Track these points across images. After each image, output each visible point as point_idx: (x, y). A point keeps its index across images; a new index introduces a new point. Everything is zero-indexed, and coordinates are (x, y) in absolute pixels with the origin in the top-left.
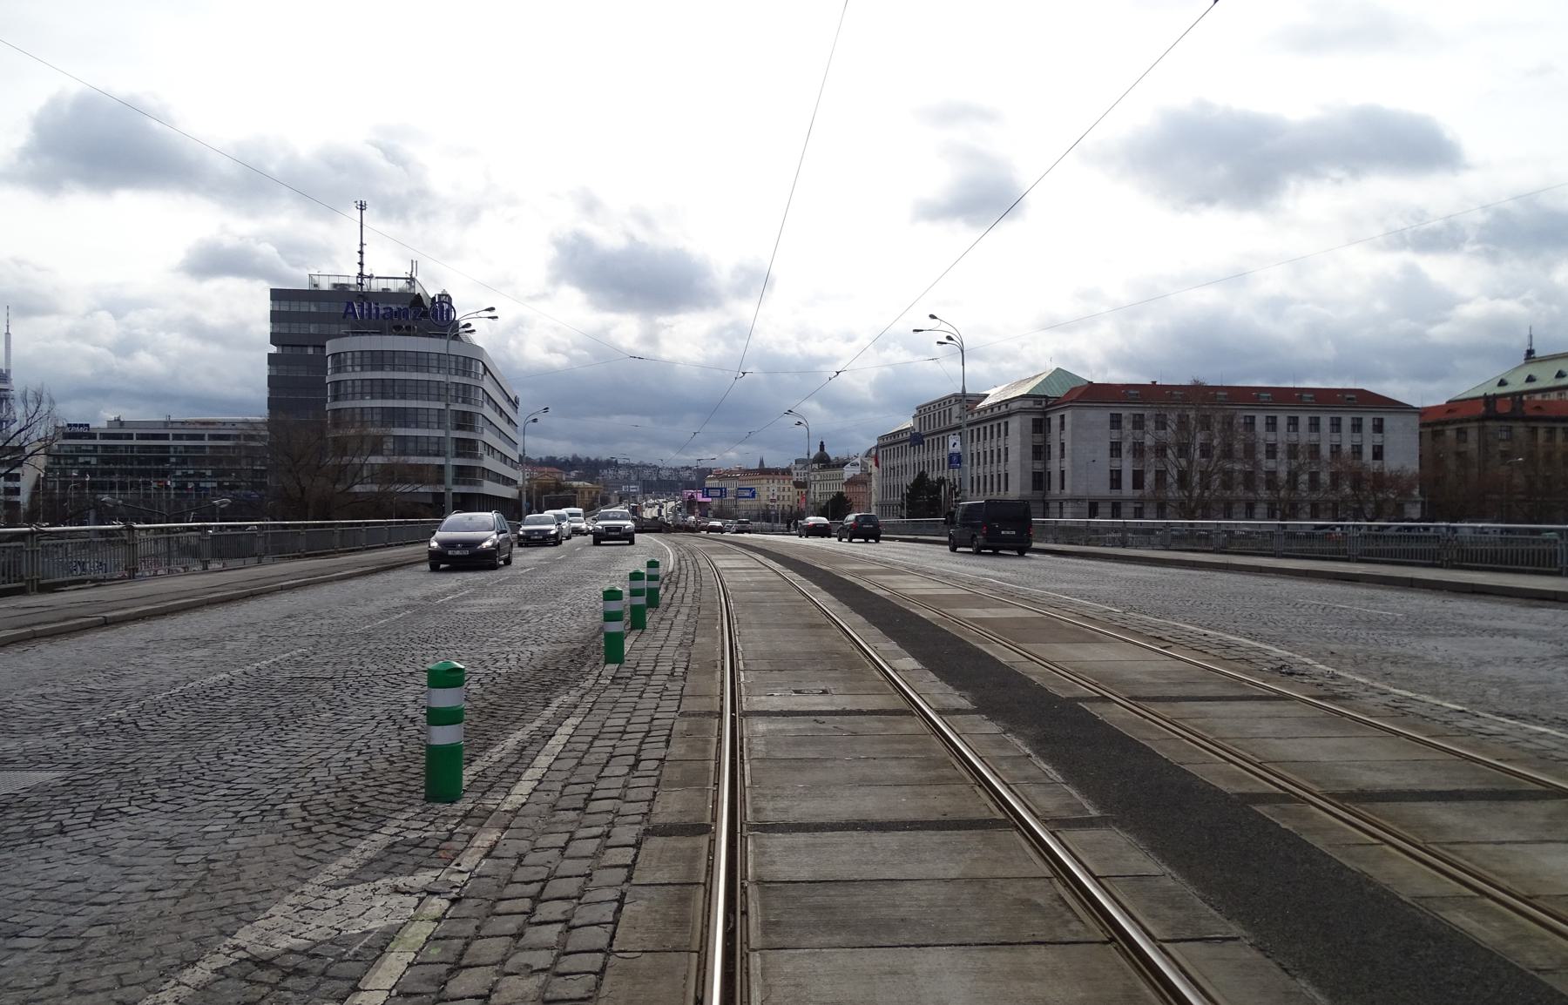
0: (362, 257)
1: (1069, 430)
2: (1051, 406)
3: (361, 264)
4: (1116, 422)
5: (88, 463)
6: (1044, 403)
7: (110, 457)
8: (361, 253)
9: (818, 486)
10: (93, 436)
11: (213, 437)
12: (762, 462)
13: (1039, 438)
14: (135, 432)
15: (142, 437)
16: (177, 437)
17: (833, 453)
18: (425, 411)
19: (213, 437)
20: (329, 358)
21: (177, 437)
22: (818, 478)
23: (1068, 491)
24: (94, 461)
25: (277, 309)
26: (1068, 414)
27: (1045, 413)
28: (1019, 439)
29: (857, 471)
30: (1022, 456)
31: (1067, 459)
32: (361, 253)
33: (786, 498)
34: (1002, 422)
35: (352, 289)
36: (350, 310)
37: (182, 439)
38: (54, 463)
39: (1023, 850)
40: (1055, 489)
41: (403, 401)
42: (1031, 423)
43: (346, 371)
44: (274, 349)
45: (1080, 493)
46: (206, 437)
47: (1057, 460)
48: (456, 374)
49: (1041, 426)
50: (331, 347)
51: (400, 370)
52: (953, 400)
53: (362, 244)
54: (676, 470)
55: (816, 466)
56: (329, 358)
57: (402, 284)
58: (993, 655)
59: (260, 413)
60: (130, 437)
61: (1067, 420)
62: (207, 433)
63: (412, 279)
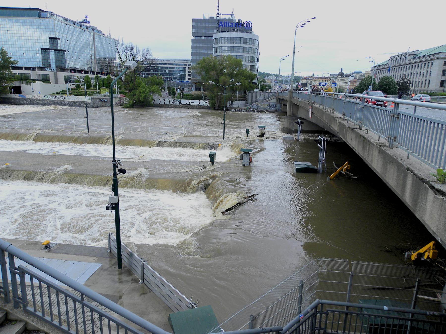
0: (218, 7)
3: (218, 10)
8: (218, 6)
9: (339, 83)
11: (170, 64)
12: (313, 75)
16: (161, 64)
17: (345, 72)
18: (242, 57)
19: (170, 64)
20: (214, 40)
21: (161, 64)
22: (339, 80)
25: (193, 52)
29: (353, 78)
32: (218, 6)
34: (430, 62)
36: (221, 24)
41: (236, 53)
43: (219, 44)
44: (193, 38)
46: (168, 64)
48: (251, 45)
50: (214, 36)
52: (408, 54)
55: (339, 76)
56: (214, 40)
58: (342, 138)
59: (189, 57)
60: (176, 64)
62: (168, 63)
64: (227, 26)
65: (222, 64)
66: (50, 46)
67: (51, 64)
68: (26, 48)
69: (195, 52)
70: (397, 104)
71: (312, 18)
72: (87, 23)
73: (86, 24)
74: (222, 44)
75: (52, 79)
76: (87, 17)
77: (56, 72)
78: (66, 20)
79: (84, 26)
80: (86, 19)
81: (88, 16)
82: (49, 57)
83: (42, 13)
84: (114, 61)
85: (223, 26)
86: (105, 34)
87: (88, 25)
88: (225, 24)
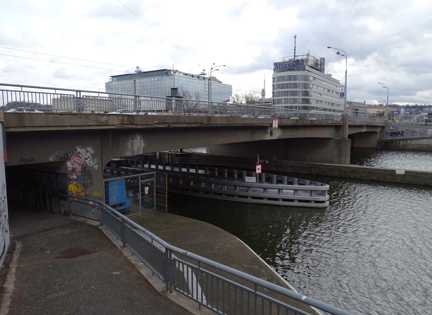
3: (295, 53)
8: (295, 50)
14: (263, 101)
53: (295, 47)
64: (281, 67)
65: (252, 98)
66: (106, 90)
70: (308, 112)
72: (205, 75)
74: (276, 82)
76: (204, 70)
78: (186, 74)
79: (201, 77)
80: (203, 72)
81: (206, 69)
85: (279, 67)
86: (222, 81)
88: (280, 66)
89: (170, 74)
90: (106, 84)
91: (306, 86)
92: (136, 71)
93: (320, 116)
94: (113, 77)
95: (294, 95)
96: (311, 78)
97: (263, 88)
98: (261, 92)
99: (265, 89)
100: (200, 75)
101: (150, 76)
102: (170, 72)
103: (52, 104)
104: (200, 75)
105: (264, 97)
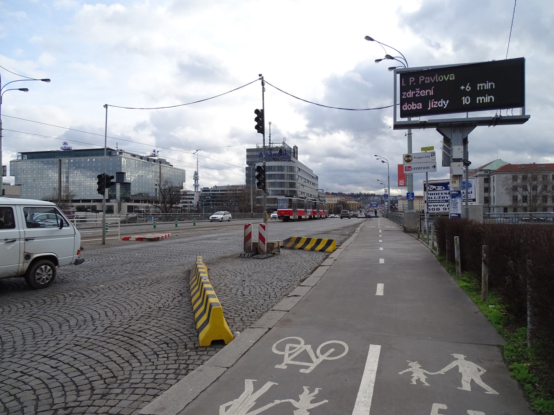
1: (496, 182)
2: (491, 173)
3: (270, 140)
4: (515, 178)
5: (208, 198)
6: (489, 172)
7: (214, 196)
8: (270, 137)
10: (209, 191)
11: (221, 191)
13: (487, 185)
14: (219, 189)
15: (221, 191)
23: (495, 203)
24: (210, 198)
25: (248, 154)
26: (495, 176)
27: (489, 176)
28: (479, 185)
30: (480, 191)
31: (495, 192)
33: (423, 206)
35: (268, 147)
37: (139, 202)
38: (200, 199)
39: (132, 249)
40: (492, 203)
42: (483, 180)
44: (247, 166)
45: (499, 204)
47: (493, 193)
49: (487, 180)
51: (274, 171)
53: (270, 134)
54: (396, 197)
57: (281, 145)
60: (218, 191)
61: (495, 178)
63: (284, 143)
67: (117, 195)
68: (90, 183)
69: (250, 154)
71: (20, 89)
73: (154, 158)
75: (115, 208)
77: (121, 203)
79: (152, 159)
82: (120, 192)
83: (112, 152)
84: (181, 190)
87: (156, 158)
89: (114, 155)
90: (11, 162)
91: (292, 177)
92: (62, 148)
93: (354, 206)
94: (23, 154)
95: (281, 187)
96: (297, 169)
97: (196, 171)
98: (193, 175)
99: (198, 172)
100: (150, 156)
101: (84, 156)
102: (114, 152)
103: (158, 196)
104: (150, 156)
105: (198, 181)
